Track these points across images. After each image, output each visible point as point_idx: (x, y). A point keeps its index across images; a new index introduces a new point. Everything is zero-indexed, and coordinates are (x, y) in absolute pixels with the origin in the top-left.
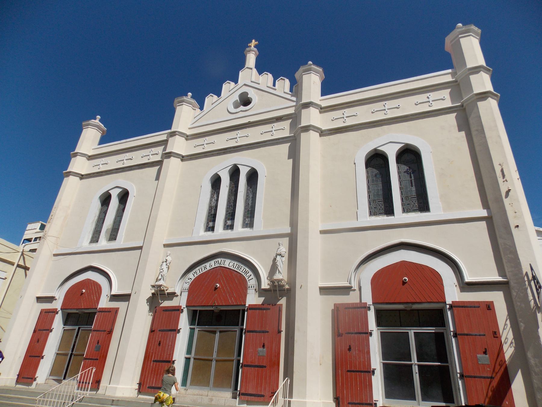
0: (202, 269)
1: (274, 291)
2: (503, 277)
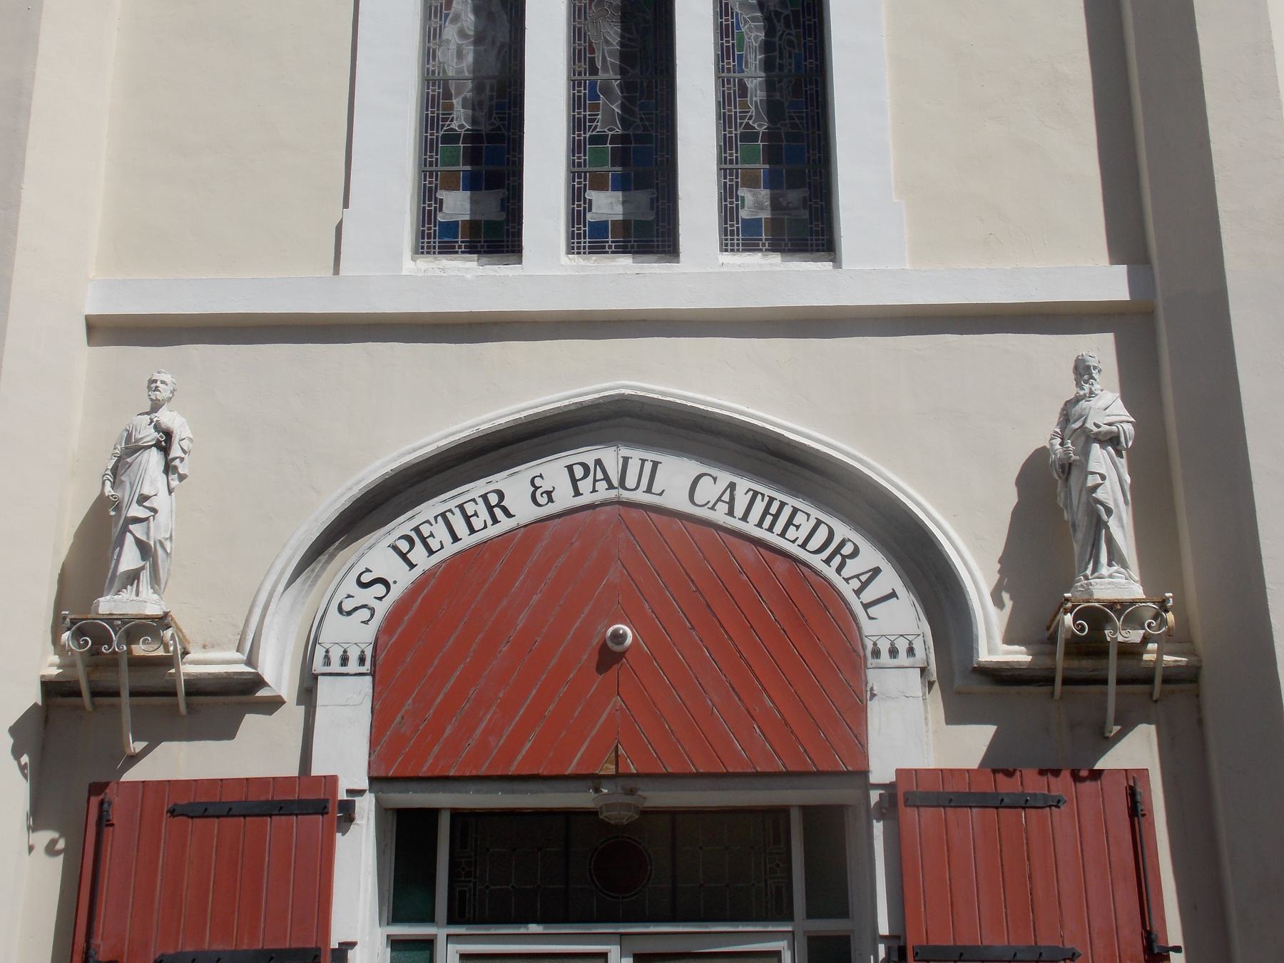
0: (467, 519)
1: (95, 694)
2: (1030, 644)
